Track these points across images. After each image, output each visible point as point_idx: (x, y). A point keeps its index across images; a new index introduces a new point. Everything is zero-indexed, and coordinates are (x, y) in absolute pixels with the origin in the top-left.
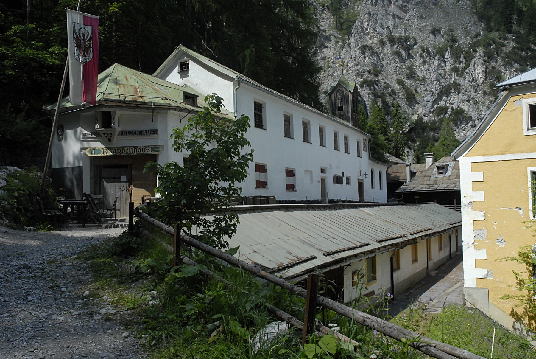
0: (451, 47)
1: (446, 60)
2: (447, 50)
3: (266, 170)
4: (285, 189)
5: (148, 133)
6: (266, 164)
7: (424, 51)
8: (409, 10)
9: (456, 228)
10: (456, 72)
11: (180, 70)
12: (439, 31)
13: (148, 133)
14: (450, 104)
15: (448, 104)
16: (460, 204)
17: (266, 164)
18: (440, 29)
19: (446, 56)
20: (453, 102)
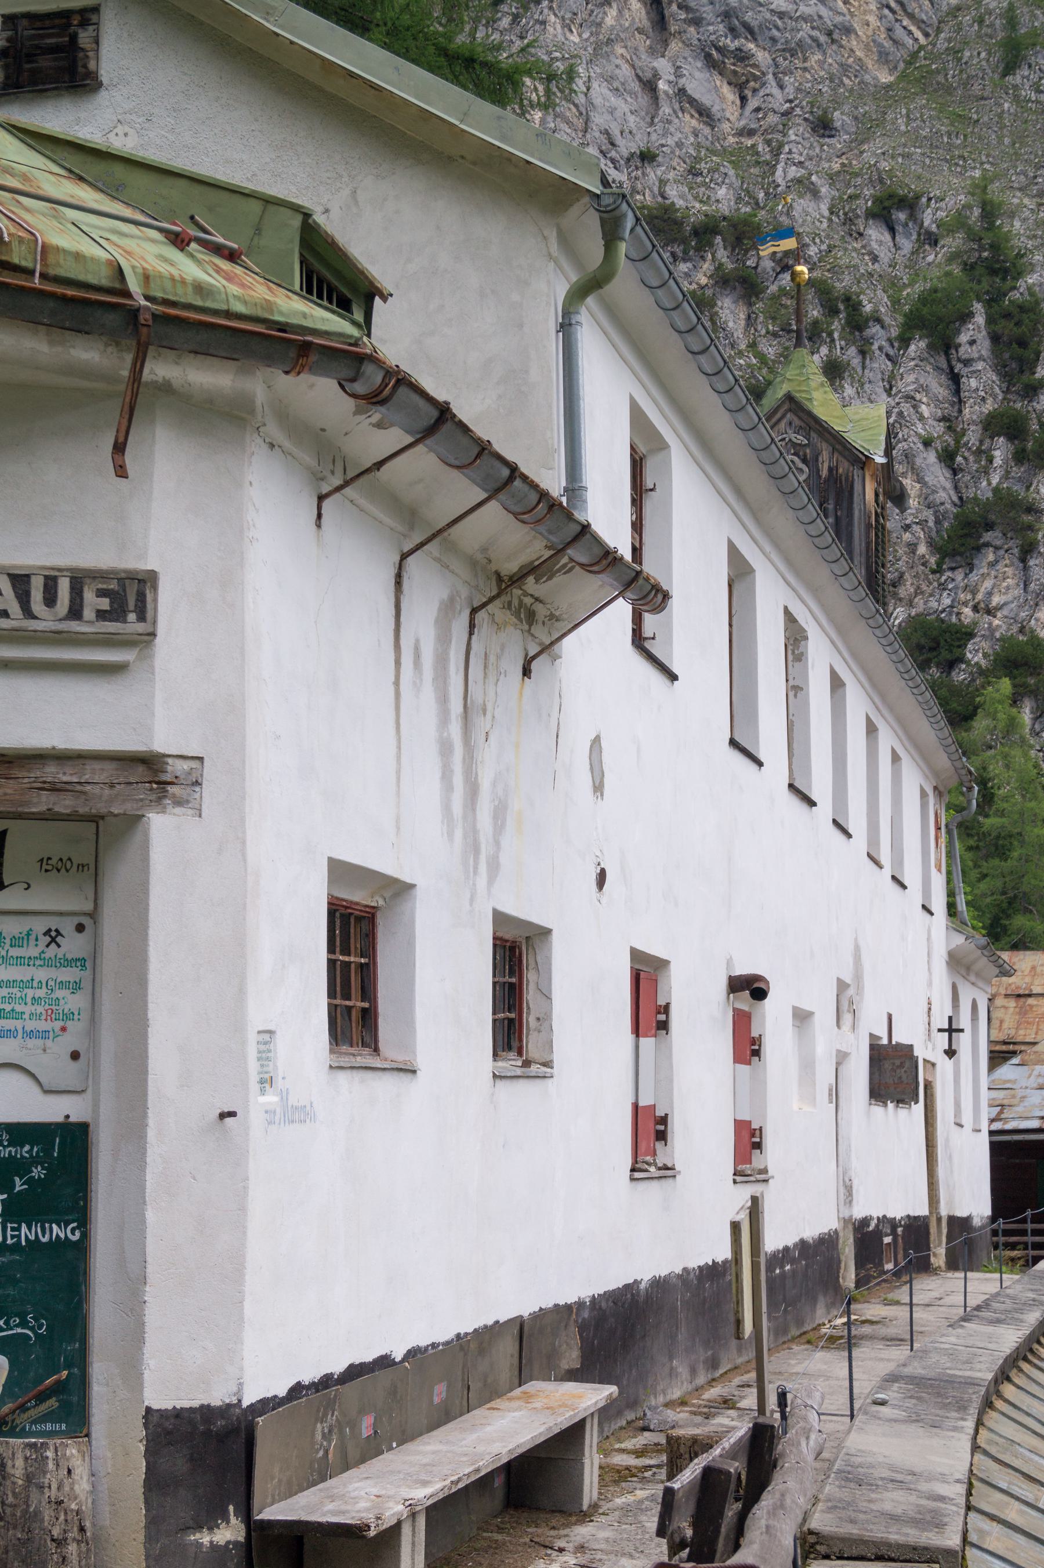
0: (992, 301)
1: (958, 367)
2: (966, 316)
3: (666, 1009)
4: (9, 838)
5: (50, 600)
6: (545, 933)
7: (833, 312)
8: (756, 78)
9: (92, 866)
10: (1011, 438)
11: (84, 38)
12: (910, 204)
13: (50, 600)
14: (976, 609)
15: (967, 611)
16: (992, 1144)
17: (545, 933)
18: (918, 198)
19: (965, 351)
20: (996, 600)
